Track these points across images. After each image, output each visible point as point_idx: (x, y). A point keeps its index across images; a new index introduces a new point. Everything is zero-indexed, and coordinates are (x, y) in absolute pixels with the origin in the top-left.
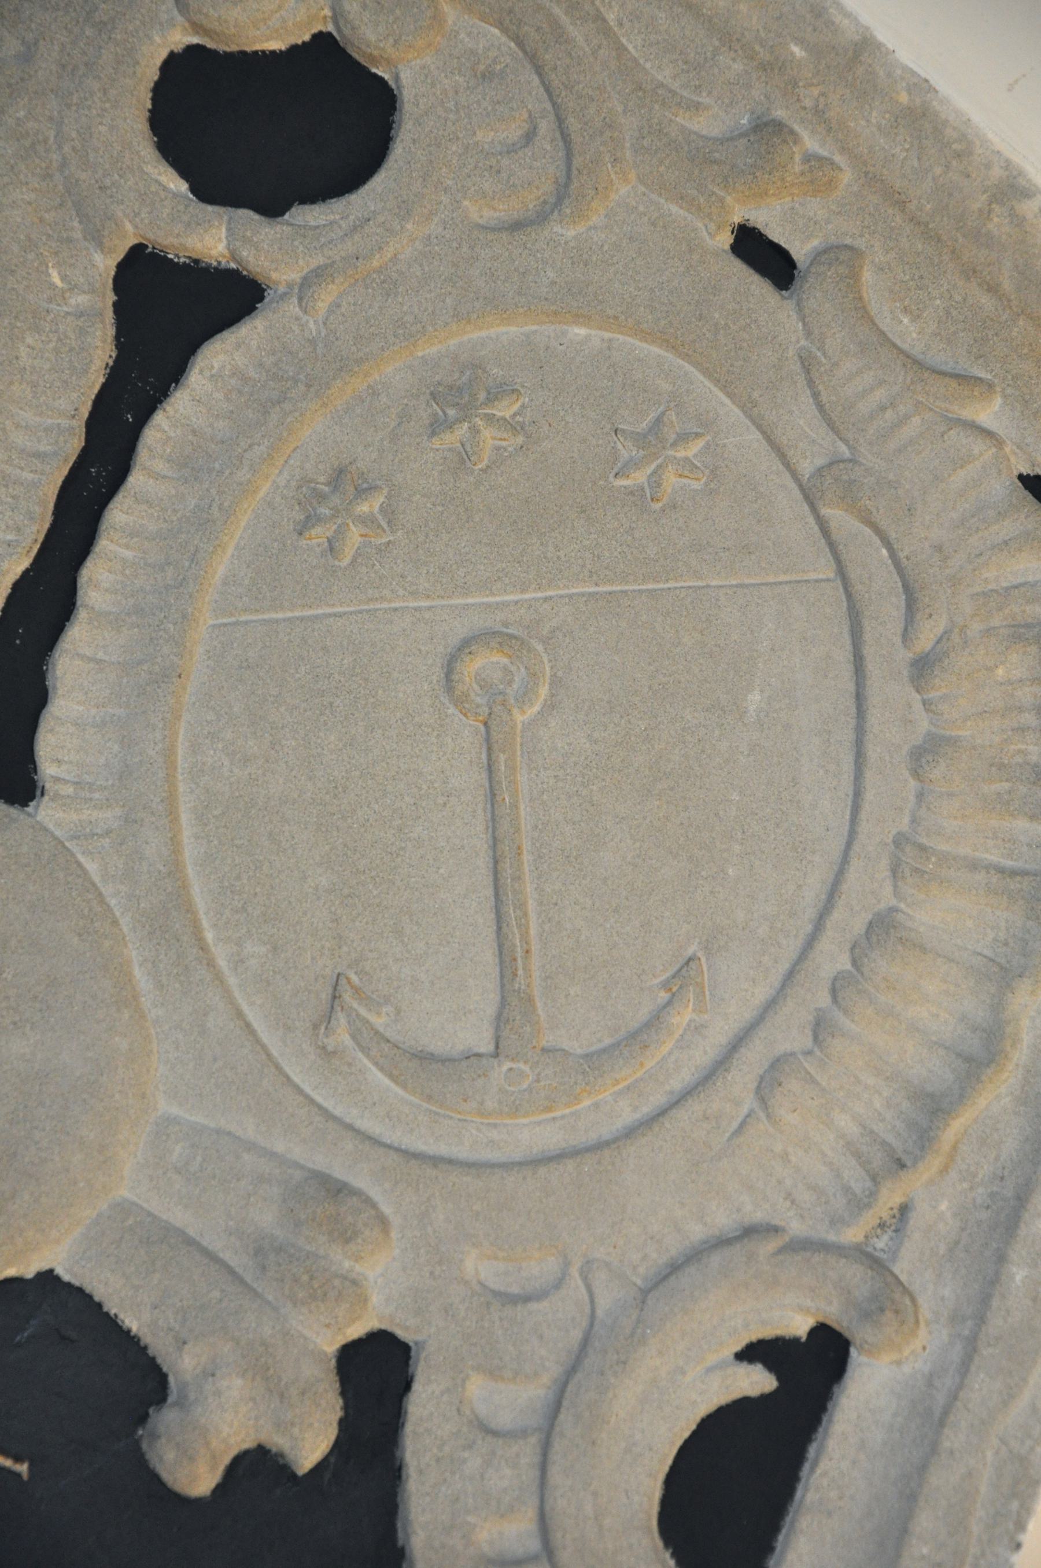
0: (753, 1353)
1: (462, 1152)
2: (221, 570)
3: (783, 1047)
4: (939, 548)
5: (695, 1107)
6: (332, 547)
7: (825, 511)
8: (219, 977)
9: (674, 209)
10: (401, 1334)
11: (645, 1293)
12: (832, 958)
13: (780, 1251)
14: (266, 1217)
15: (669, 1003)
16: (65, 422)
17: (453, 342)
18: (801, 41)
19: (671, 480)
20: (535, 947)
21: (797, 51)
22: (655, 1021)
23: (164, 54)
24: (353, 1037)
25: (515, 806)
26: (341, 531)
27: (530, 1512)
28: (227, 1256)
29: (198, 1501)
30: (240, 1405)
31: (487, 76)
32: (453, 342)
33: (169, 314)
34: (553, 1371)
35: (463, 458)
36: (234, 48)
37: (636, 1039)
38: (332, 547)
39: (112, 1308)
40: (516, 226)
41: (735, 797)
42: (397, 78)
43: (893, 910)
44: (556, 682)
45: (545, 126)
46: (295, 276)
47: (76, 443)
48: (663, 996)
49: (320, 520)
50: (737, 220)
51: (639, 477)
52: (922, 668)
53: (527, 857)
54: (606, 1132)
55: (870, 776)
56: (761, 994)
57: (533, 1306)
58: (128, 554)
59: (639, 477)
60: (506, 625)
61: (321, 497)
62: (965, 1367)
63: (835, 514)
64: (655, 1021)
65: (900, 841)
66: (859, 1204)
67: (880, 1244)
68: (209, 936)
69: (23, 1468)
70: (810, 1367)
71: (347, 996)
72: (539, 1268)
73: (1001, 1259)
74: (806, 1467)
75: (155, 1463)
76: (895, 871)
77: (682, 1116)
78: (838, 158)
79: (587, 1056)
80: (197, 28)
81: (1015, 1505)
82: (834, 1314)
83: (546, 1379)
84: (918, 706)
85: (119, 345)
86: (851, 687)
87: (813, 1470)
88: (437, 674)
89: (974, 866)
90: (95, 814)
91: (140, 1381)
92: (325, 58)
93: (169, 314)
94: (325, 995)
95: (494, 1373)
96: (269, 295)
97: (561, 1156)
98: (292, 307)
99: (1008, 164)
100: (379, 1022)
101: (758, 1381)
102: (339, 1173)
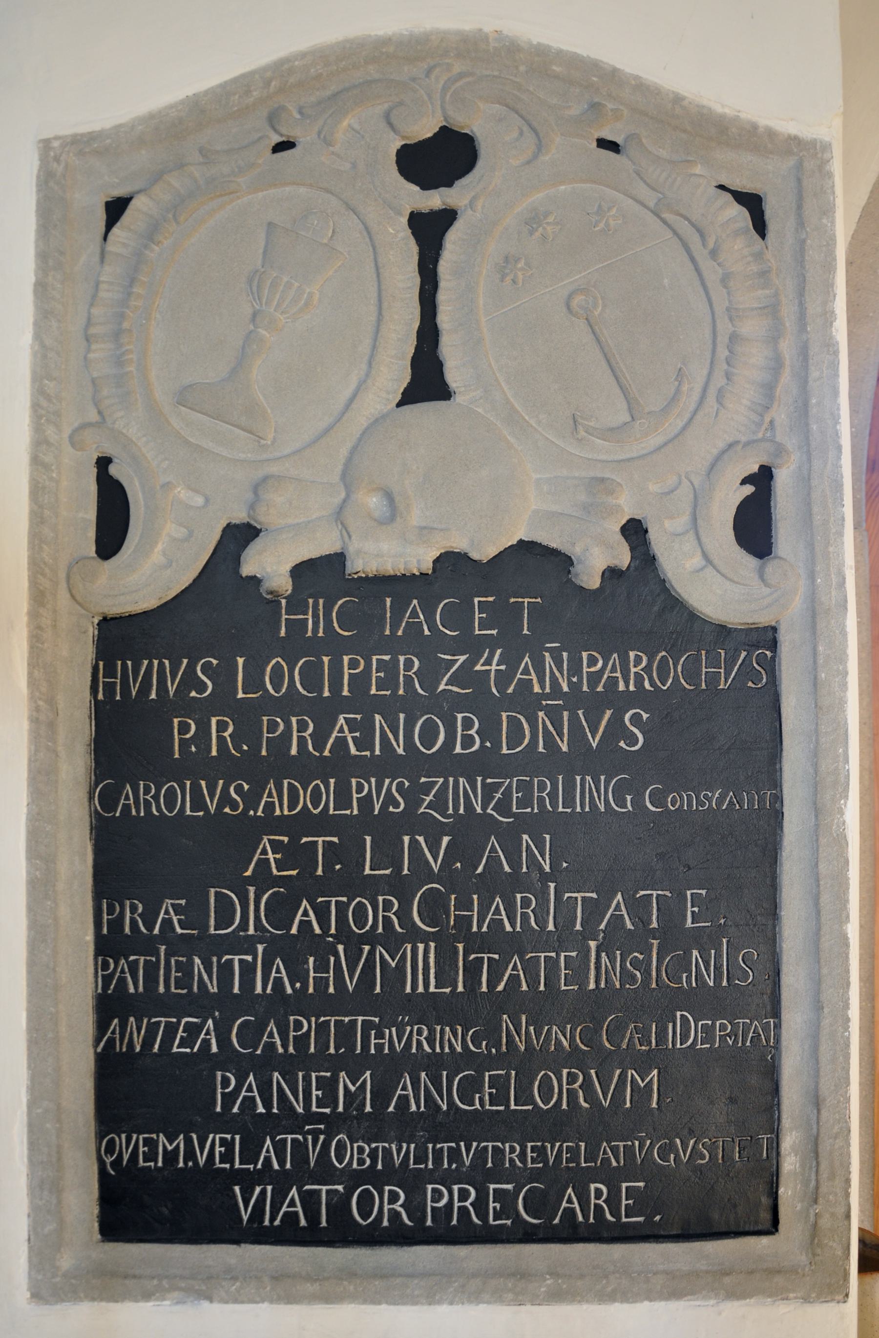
0: (744, 482)
1: (634, 455)
2: (481, 302)
3: (719, 386)
4: (703, 215)
5: (701, 414)
6: (514, 281)
7: (663, 216)
8: (535, 429)
9: (576, 140)
10: (637, 517)
11: (709, 474)
12: (723, 353)
13: (743, 447)
14: (582, 497)
15: (680, 384)
16: (413, 275)
17: (524, 205)
18: (595, 76)
19: (612, 223)
20: (631, 382)
21: (595, 79)
22: (678, 391)
23: (395, 151)
24: (586, 432)
25: (607, 341)
26: (516, 276)
27: (699, 553)
28: (574, 514)
29: (597, 589)
30: (597, 556)
31: (500, 120)
32: (524, 205)
33: (430, 230)
34: (689, 510)
35: (544, 237)
36: (417, 141)
37: (675, 398)
38: (514, 281)
39: (545, 543)
40: (529, 162)
41: (673, 313)
42: (472, 131)
43: (734, 331)
44: (602, 298)
45: (525, 128)
46: (466, 202)
47: (418, 280)
48: (677, 383)
49: (507, 274)
50: (596, 137)
51: (602, 225)
52: (714, 254)
53: (617, 356)
54: (676, 431)
55: (712, 293)
56: (705, 372)
57: (675, 493)
58: (449, 308)
59: (602, 225)
60: (579, 286)
61: (504, 267)
62: (809, 460)
63: (665, 215)
64: (678, 391)
65: (728, 309)
66: (759, 425)
67: (768, 435)
68: (527, 418)
69: (539, 600)
70: (762, 479)
71: (579, 420)
72: (672, 481)
73: (807, 425)
74: (772, 509)
75: (578, 582)
76: (731, 319)
77: (698, 417)
78: (621, 107)
79: (662, 410)
80: (404, 138)
81: (838, 494)
82: (765, 460)
83: (688, 513)
84: (716, 266)
85: (419, 245)
86: (693, 268)
87: (775, 508)
88: (565, 309)
89: (752, 309)
90: (474, 394)
91: (562, 561)
92: (446, 134)
93: (430, 230)
94: (572, 422)
95: (671, 517)
96: (459, 212)
97: (665, 444)
98: (470, 212)
99: (673, 92)
100: (592, 424)
101: (749, 489)
102: (599, 475)
